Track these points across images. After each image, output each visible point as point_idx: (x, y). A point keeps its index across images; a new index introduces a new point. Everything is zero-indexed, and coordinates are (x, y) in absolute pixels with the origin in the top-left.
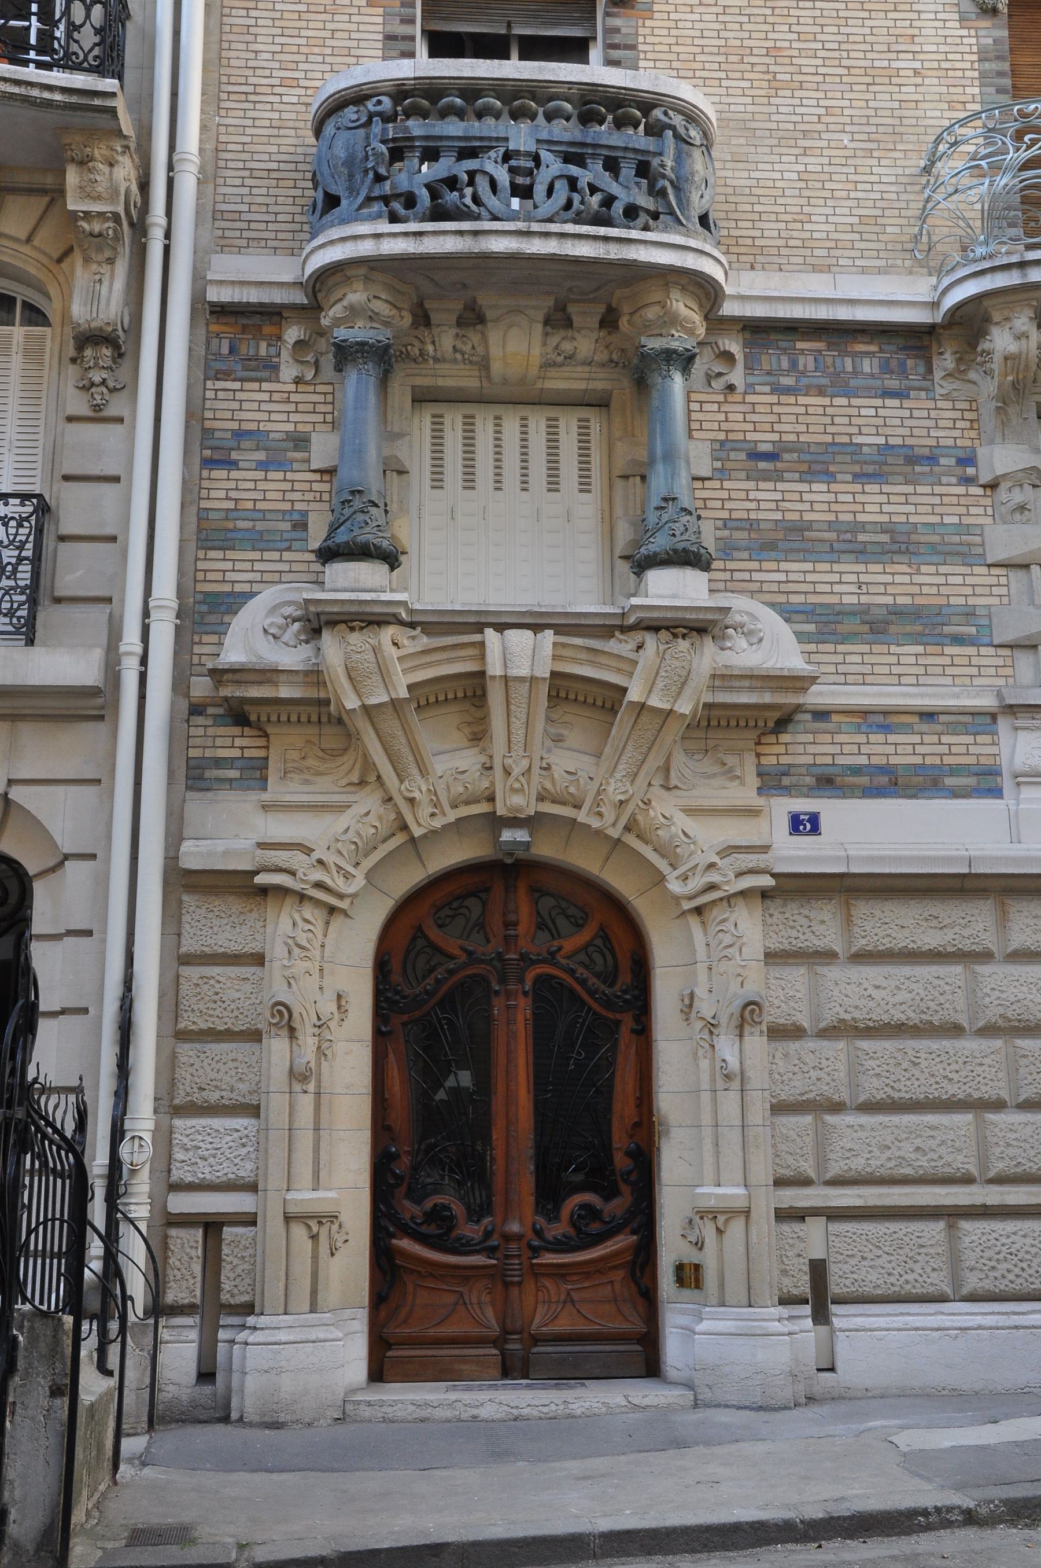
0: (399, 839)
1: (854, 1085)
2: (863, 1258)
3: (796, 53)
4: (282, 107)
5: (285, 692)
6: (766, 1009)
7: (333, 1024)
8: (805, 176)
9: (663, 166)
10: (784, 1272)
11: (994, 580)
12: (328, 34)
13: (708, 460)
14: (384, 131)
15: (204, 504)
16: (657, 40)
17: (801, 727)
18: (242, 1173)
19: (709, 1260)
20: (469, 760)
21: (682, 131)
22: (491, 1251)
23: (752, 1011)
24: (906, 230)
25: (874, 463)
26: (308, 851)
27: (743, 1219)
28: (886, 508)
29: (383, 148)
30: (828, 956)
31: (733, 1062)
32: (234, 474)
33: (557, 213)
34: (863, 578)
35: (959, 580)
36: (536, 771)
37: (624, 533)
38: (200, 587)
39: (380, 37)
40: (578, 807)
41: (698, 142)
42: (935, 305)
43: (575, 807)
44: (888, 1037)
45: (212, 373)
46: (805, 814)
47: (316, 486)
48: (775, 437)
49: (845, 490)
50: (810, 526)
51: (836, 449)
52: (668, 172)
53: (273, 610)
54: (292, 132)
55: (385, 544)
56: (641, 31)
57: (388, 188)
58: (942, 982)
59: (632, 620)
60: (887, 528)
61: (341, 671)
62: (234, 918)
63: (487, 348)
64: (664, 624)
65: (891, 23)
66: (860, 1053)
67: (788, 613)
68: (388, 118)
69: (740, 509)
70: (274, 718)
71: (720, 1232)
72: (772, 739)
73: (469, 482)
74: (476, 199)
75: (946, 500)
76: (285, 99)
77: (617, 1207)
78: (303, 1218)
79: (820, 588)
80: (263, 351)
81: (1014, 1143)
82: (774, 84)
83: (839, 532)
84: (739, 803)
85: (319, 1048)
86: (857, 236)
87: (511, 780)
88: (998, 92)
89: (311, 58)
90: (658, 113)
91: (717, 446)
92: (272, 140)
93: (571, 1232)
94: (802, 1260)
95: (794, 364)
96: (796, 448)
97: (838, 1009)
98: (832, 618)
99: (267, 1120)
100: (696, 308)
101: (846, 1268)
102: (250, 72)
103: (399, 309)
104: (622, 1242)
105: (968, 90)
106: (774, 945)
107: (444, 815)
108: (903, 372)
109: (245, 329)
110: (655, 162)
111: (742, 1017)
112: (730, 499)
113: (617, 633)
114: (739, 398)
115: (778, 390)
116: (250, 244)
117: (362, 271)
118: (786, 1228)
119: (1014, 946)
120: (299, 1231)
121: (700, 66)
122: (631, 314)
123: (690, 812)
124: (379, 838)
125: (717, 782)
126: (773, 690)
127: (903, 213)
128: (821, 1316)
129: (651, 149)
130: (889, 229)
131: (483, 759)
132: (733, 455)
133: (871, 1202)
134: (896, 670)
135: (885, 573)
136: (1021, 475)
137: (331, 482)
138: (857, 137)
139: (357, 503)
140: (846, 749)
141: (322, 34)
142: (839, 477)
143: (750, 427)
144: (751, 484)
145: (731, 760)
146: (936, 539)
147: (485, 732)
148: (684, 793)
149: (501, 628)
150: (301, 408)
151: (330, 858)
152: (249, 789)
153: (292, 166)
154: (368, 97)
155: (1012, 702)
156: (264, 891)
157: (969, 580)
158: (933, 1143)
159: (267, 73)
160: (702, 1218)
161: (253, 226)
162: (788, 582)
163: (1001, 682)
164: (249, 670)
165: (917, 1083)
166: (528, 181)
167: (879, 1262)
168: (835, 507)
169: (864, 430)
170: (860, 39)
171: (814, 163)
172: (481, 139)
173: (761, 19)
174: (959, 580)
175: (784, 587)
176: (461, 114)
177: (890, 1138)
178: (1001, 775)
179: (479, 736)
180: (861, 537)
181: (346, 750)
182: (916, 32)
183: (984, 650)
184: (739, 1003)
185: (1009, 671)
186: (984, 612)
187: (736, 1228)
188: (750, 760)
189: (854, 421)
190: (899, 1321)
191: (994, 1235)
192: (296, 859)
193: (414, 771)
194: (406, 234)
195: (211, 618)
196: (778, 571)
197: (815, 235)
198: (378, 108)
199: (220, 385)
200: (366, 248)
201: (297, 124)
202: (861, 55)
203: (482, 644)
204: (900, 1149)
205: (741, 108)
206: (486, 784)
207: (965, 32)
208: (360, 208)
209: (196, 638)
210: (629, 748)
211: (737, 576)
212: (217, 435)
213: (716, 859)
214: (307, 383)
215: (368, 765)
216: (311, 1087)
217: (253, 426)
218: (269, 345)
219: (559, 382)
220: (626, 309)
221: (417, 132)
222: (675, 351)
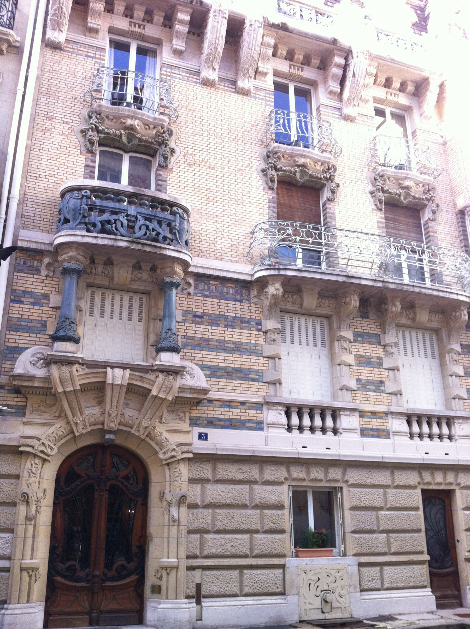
0: (71, 436)
1: (213, 524)
4: (48, 183)
5: (36, 384)
7: (42, 500)
10: (188, 588)
11: (264, 362)
15: (10, 315)
17: (204, 405)
18: (6, 553)
19: (163, 584)
20: (96, 411)
21: (182, 215)
22: (88, 581)
26: (39, 439)
27: (175, 570)
28: (234, 336)
30: (207, 481)
31: (176, 516)
32: (22, 306)
34: (226, 358)
35: (254, 361)
36: (119, 415)
37: (152, 338)
38: (6, 344)
40: (131, 428)
42: (252, 275)
44: (225, 508)
45: (17, 270)
47: (50, 313)
48: (202, 311)
49: (222, 329)
50: (210, 340)
52: (177, 228)
53: (33, 355)
54: (51, 192)
55: (76, 337)
60: (234, 343)
63: (113, 273)
67: (202, 367)
69: (190, 333)
70: (31, 392)
71: (168, 574)
72: (195, 408)
73: (102, 315)
74: (116, 228)
75: (252, 335)
77: (132, 565)
78: (27, 569)
79: (212, 360)
80: (35, 265)
84: (183, 429)
90: (175, 208)
91: (184, 312)
93: (116, 574)
95: (209, 288)
96: (208, 315)
99: (16, 534)
102: (38, 170)
103: (86, 258)
104: (133, 578)
106: (191, 477)
108: (241, 294)
109: (29, 256)
110: (173, 224)
115: (204, 296)
116: (33, 227)
118: (189, 573)
119: (265, 479)
120: (25, 574)
123: (168, 431)
124: (64, 435)
125: (176, 422)
128: (198, 602)
131: (102, 410)
132: (188, 315)
134: (234, 388)
139: (67, 322)
141: (64, 161)
142: (220, 325)
143: (194, 307)
144: (193, 325)
145: (182, 415)
146: (248, 347)
149: (112, 367)
150: (47, 285)
151: (47, 442)
152: (18, 416)
153: (50, 203)
156: (22, 453)
157: (257, 361)
158: (237, 544)
161: (35, 221)
163: (265, 394)
166: (133, 224)
167: (218, 584)
168: (218, 335)
169: (229, 311)
171: (219, 226)
172: (119, 209)
174: (254, 361)
175: (201, 359)
176: (112, 199)
177: (223, 543)
179: (101, 402)
180: (226, 345)
183: (261, 384)
184: (179, 496)
185: (267, 391)
186: (261, 371)
189: (226, 308)
190: (222, 604)
193: (79, 413)
194: (92, 237)
195: (10, 355)
198: (86, 194)
199: (19, 274)
200: (79, 239)
206: (102, 419)
208: (77, 225)
209: (4, 362)
210: (150, 409)
211: (187, 354)
212: (17, 291)
213: (175, 448)
214: (50, 277)
215: (62, 410)
216: (33, 523)
217: (30, 290)
219: (134, 286)
220: (159, 267)
221: (98, 204)
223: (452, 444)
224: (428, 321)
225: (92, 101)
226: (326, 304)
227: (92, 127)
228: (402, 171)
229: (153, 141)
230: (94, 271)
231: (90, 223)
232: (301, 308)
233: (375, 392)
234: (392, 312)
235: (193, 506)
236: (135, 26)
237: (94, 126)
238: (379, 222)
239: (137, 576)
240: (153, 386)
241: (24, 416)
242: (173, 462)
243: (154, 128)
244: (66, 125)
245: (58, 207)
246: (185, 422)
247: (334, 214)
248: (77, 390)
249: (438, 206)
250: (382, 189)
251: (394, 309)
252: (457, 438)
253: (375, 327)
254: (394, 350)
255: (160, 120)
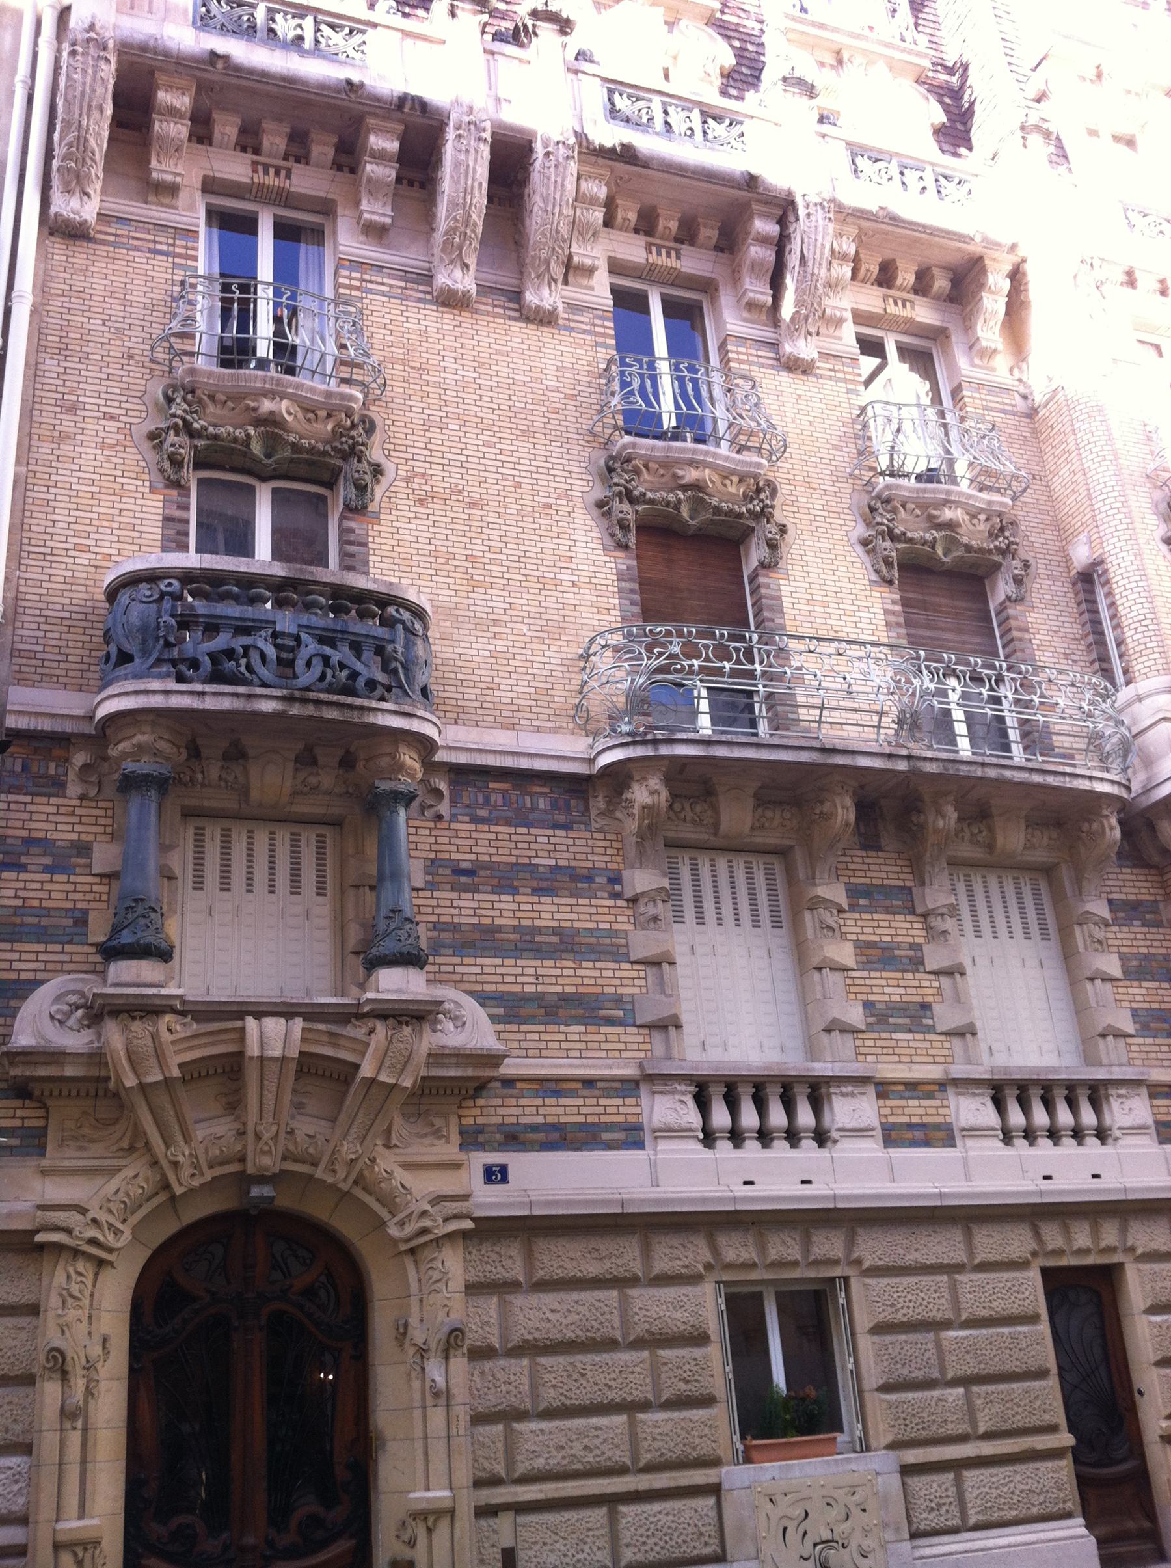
0: (162, 1197)
1: (535, 1395)
2: (545, 1544)
3: (487, 561)
4: (74, 567)
5: (69, 1072)
6: (468, 1334)
8: (494, 654)
9: (395, 651)
11: (635, 974)
12: (117, 512)
13: (422, 875)
14: (174, 607)
16: (383, 541)
20: (224, 1127)
21: (409, 624)
23: (457, 1337)
24: (569, 700)
25: (546, 879)
26: (83, 1211)
28: (557, 916)
29: (173, 621)
30: (512, 1286)
31: (440, 1380)
32: (23, 876)
33: (314, 683)
34: (540, 971)
35: (611, 974)
36: (282, 1135)
37: (354, 935)
39: (161, 518)
41: (420, 633)
42: (591, 761)
43: (312, 1164)
46: (497, 1166)
47: (95, 888)
48: (473, 857)
49: (526, 901)
50: (499, 928)
51: (519, 868)
52: (400, 657)
53: (58, 999)
56: (371, 533)
57: (176, 653)
58: (602, 1305)
59: (366, 1009)
60: (557, 931)
61: (122, 1054)
62: (12, 1272)
64: (392, 1013)
65: (556, 547)
66: (539, 1368)
67: (483, 999)
68: (178, 597)
69: (447, 915)
70: (56, 1093)
71: (430, 1530)
72: (470, 1103)
73: (225, 886)
74: (249, 668)
75: (600, 910)
76: (78, 561)
79: (507, 979)
81: (659, 1437)
82: (471, 583)
83: (522, 934)
85: (87, 1387)
86: (534, 703)
87: (261, 1143)
88: (632, 604)
89: (101, 530)
90: (391, 610)
91: (429, 863)
92: (65, 594)
94: (495, 1549)
95: (487, 800)
97: (523, 1331)
98: (516, 1004)
100: (416, 757)
101: (531, 1553)
102: (48, 537)
103: (178, 747)
105: (611, 600)
106: (472, 1278)
107: (202, 1174)
108: (568, 810)
109: (36, 751)
110: (390, 647)
111: (448, 1342)
112: (438, 906)
113: (353, 1020)
114: (446, 825)
115: (475, 820)
116: (41, 679)
117: (151, 717)
118: (483, 1523)
119: (656, 1271)
121: (416, 564)
122: (367, 761)
123: (407, 1166)
124: (145, 1197)
125: (427, 1141)
126: (475, 1066)
127: (567, 687)
129: (386, 637)
130: (557, 699)
131: (237, 1125)
132: (441, 871)
133: (550, 1495)
134: (564, 1045)
135: (556, 967)
136: (653, 893)
137: (109, 884)
138: (532, 627)
139: (140, 910)
140: (528, 1110)
141: (112, 511)
144: (454, 895)
145: (439, 1122)
146: (594, 940)
147: (240, 1101)
148: (402, 1151)
149: (258, 1015)
151: (103, 1217)
152: (28, 1155)
154: (160, 578)
155: (651, 1072)
156: (41, 1247)
157: (618, 974)
158: (597, 1442)
159: (63, 539)
160: (414, 1519)
162: (482, 974)
163: (642, 1055)
164: (38, 1053)
165: (584, 1391)
166: (291, 656)
167: (558, 1545)
168: (518, 914)
170: (534, 555)
171: (502, 646)
172: (253, 620)
173: (461, 533)
174: (611, 974)
175: (479, 978)
176: (236, 598)
178: (643, 1130)
179: (234, 1105)
180: (538, 939)
181: (117, 1119)
182: (573, 555)
183: (630, 1030)
184: (446, 1330)
185: (647, 1046)
187: (443, 1527)
188: (454, 1121)
191: (645, 1515)
192: (72, 1219)
193: (179, 1138)
196: (475, 965)
197: (503, 700)
198: (169, 589)
200: (157, 701)
201: (88, 582)
202: (535, 567)
203: (243, 1030)
204: (571, 1448)
205: (447, 599)
206: (238, 1147)
207: (607, 559)
208: (151, 667)
210: (360, 1115)
211: (444, 968)
212: (9, 841)
213: (428, 1207)
214: (91, 799)
215: (138, 1132)
216: (79, 1424)
217: (41, 835)
218: (57, 766)
219: (302, 808)
221: (201, 611)
222: (401, 793)
223: (1107, 1150)
224: (1025, 848)
225: (171, 361)
226: (776, 822)
227: (176, 424)
228: (934, 486)
229: (328, 448)
230: (200, 776)
231: (183, 660)
232: (716, 834)
233: (910, 1031)
234: (936, 831)
235: (481, 1353)
236: (266, 173)
237: (622, 489)
238: (887, 612)
239: (354, 1541)
240: (363, 1054)
241: (42, 1154)
242: (425, 1244)
243: (329, 416)
244: (111, 423)
245: (101, 626)
246: (448, 1142)
247: (779, 598)
248: (172, 1078)
249: (1026, 565)
250: (890, 531)
251: (941, 823)
252: (1118, 1133)
253: (898, 869)
254: (949, 924)
255: (343, 397)
